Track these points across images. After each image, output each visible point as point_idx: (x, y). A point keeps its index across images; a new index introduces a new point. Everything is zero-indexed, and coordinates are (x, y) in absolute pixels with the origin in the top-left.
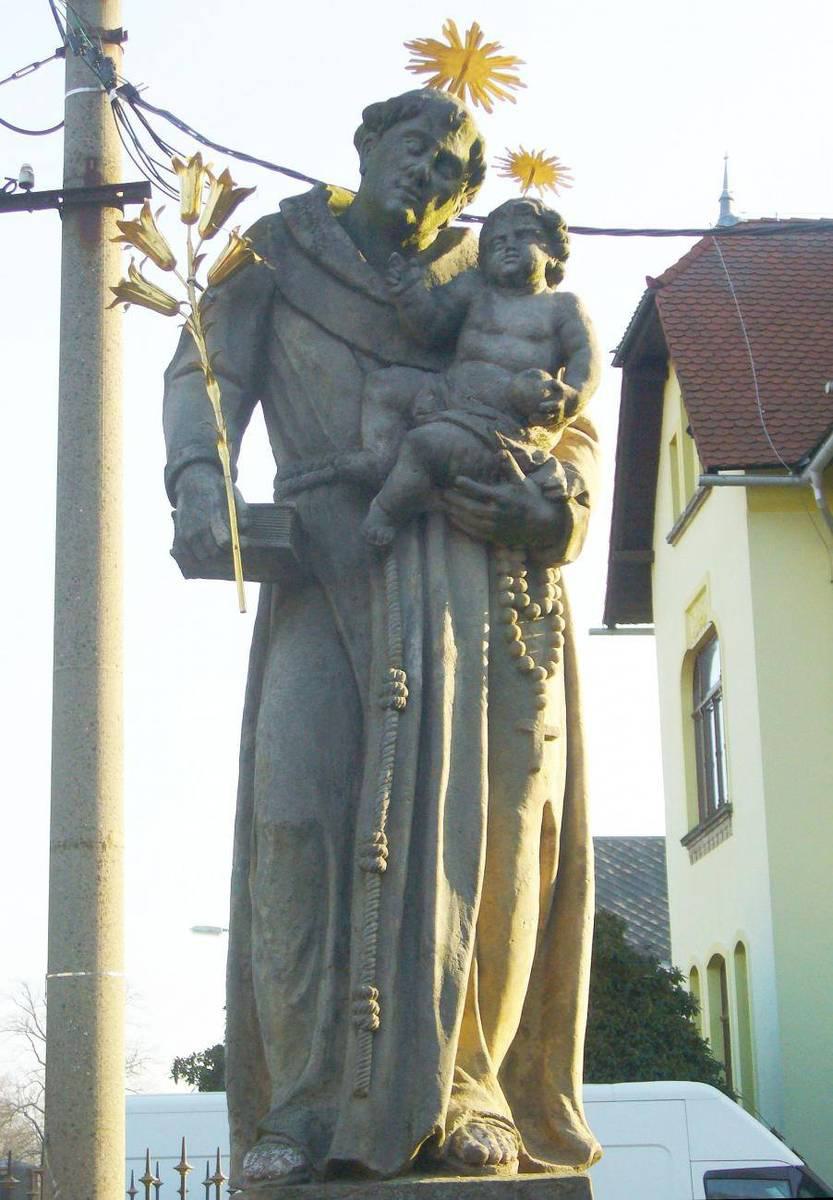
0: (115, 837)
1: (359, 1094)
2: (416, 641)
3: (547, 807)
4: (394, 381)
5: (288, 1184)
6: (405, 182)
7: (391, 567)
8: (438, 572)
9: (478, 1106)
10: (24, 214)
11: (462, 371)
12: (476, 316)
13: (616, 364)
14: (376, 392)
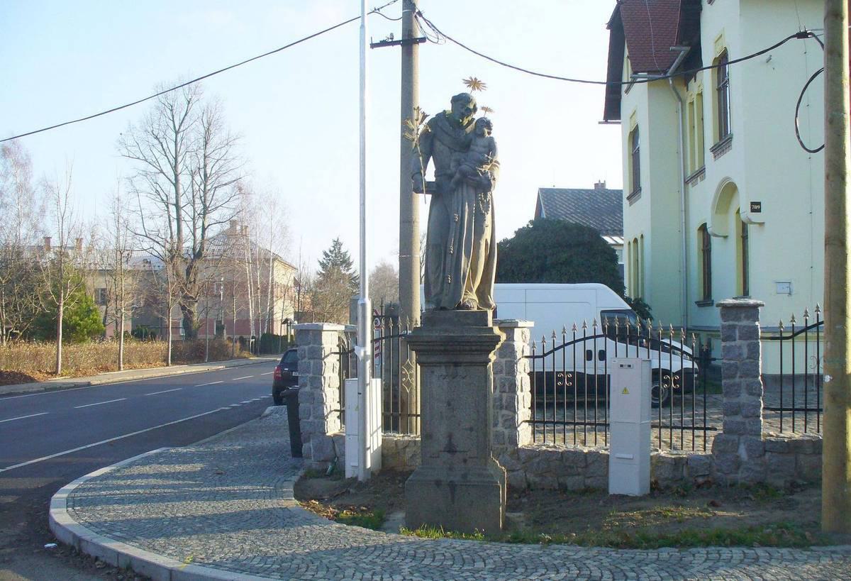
0: (417, 220)
1: (446, 295)
2: (460, 208)
3: (486, 240)
4: (457, 155)
7: (456, 193)
8: (465, 194)
9: (471, 299)
10: (391, 47)
11: (471, 153)
12: (473, 142)
13: (608, 28)
14: (453, 158)
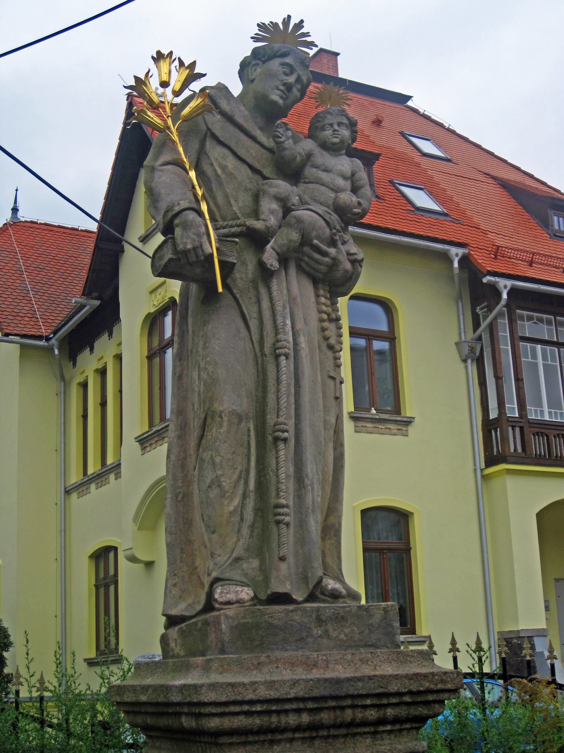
5: (251, 605)
6: (282, 88)
